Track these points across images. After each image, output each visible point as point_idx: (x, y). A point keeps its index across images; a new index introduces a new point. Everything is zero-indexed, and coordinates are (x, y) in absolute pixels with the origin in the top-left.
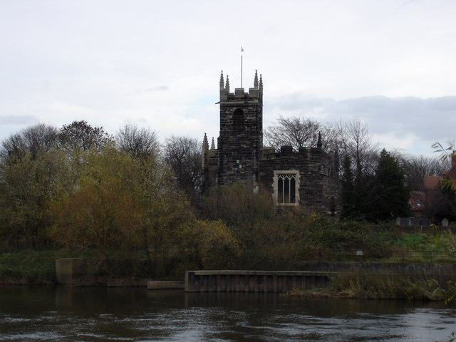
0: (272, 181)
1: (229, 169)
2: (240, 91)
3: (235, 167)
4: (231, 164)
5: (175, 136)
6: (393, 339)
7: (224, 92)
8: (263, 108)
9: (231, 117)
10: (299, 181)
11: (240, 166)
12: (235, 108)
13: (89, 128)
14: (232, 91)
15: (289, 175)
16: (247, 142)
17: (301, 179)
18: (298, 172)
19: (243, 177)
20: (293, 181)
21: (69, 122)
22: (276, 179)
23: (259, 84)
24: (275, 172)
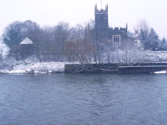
0: (112, 38)
1: (99, 35)
2: (102, 10)
3: (101, 34)
4: (100, 33)
5: (54, 25)
6: (127, 26)
7: (96, 10)
8: (94, 8)
9: (99, 18)
10: (120, 38)
11: (103, 34)
12: (101, 15)
13: (32, 22)
14: (99, 10)
15: (117, 37)
16: (105, 26)
17: (121, 38)
18: (120, 35)
19: (104, 37)
20: (118, 38)
21: (25, 20)
22: (113, 38)
23: (107, 8)
24: (113, 36)
